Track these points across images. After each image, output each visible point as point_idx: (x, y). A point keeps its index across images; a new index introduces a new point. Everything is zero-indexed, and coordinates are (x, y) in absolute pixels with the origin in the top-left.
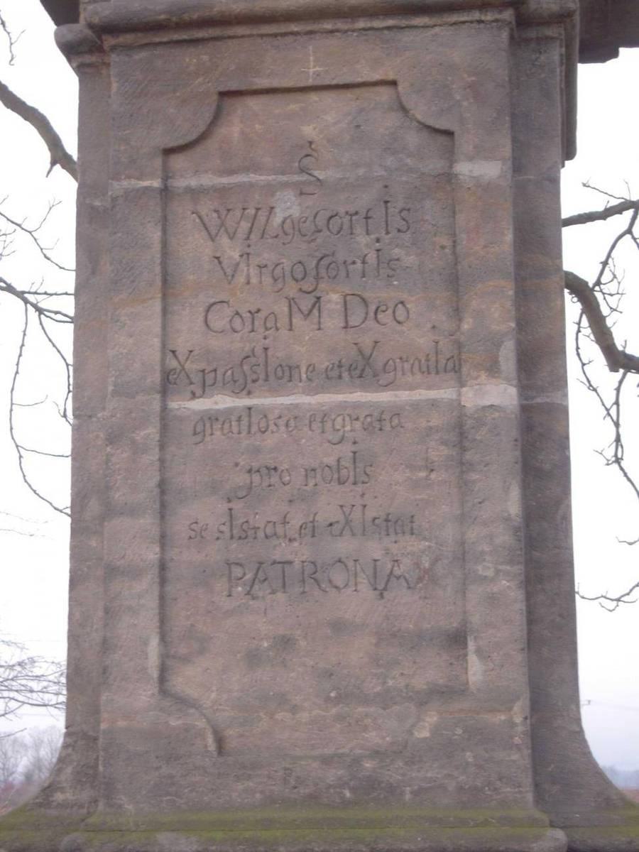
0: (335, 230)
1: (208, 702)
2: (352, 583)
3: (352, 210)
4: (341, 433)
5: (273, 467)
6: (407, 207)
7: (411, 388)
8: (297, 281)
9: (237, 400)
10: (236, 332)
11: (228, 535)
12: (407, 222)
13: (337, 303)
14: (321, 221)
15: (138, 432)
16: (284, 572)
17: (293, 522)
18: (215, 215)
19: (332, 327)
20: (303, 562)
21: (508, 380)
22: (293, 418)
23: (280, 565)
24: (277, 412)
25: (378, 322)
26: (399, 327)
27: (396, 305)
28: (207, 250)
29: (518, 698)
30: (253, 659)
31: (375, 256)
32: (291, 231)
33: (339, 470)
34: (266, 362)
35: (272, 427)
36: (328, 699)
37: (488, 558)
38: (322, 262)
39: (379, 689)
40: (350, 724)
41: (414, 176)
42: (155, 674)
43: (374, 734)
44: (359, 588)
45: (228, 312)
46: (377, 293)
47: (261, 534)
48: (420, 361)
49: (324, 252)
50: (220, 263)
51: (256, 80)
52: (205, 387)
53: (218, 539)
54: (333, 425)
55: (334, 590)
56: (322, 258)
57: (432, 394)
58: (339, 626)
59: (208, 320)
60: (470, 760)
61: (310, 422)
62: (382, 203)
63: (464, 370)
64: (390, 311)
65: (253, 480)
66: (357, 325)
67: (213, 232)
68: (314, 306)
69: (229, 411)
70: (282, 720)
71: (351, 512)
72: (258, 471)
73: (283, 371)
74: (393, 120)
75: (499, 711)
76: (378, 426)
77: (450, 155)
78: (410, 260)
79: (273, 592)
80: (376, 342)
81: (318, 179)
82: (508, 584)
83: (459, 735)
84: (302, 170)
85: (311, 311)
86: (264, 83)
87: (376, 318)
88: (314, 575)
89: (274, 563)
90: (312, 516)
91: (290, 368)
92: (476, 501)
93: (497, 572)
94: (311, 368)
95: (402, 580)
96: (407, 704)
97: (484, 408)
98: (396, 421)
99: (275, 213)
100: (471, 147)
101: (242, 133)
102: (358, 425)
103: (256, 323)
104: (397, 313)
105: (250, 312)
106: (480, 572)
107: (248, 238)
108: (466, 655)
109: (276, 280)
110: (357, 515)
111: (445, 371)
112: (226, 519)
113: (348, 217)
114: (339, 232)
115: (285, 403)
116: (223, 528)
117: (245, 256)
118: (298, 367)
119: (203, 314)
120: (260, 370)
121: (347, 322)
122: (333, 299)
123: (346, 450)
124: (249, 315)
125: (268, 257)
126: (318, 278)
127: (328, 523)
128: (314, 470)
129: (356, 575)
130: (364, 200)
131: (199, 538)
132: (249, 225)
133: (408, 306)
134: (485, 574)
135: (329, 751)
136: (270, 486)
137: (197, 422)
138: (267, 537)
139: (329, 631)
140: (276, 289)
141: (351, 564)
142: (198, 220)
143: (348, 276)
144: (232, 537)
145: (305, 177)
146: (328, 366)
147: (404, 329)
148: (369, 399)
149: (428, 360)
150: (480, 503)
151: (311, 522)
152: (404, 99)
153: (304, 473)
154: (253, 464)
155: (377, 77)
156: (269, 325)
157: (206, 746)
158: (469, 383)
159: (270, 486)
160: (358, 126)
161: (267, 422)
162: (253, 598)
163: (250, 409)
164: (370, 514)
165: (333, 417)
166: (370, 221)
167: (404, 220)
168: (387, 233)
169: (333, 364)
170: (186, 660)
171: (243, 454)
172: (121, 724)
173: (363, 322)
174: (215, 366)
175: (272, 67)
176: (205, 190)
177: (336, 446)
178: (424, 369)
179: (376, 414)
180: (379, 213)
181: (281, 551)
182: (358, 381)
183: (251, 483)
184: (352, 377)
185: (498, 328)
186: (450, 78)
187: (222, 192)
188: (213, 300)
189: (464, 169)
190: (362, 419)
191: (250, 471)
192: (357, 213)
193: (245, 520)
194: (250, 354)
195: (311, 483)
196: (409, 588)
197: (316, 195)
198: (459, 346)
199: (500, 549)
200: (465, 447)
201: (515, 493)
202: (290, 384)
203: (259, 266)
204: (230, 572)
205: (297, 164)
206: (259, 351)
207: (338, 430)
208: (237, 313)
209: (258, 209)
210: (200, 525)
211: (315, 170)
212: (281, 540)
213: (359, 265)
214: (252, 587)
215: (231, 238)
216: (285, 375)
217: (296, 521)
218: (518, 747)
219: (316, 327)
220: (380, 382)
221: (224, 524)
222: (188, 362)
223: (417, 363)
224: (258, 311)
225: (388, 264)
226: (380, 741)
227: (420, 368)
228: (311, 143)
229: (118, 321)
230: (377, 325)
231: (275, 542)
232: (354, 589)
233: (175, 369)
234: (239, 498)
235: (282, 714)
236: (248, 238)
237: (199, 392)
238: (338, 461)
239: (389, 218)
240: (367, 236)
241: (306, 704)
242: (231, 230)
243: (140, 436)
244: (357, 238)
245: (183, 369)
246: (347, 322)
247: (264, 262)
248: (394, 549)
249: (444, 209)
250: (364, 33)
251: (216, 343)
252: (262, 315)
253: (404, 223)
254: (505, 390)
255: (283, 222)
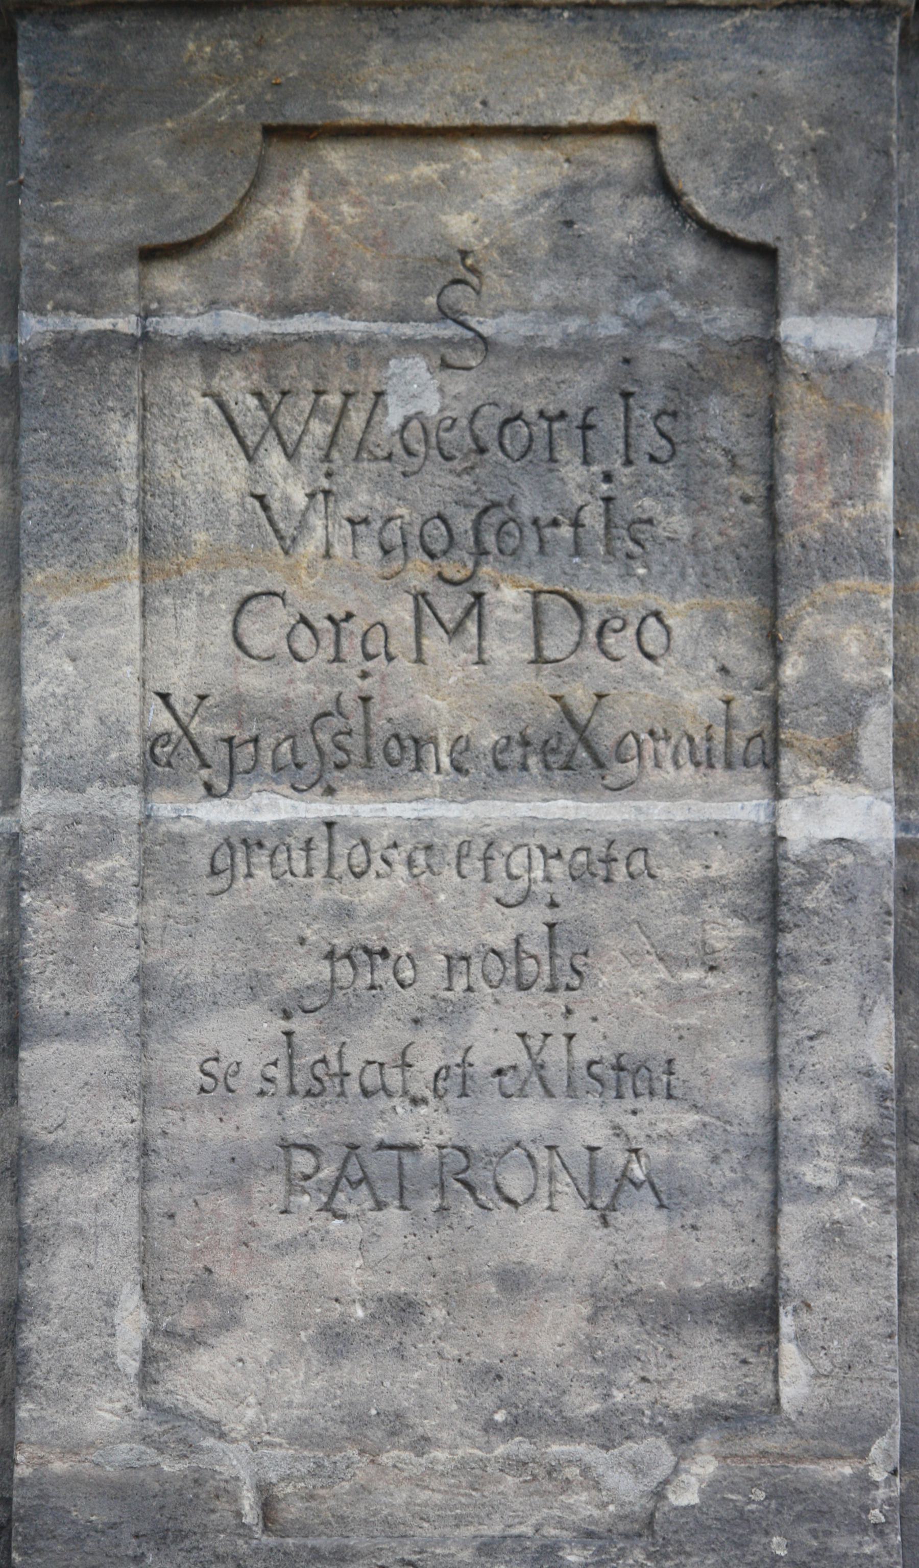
0: (515, 449)
1: (240, 1427)
2: (543, 1192)
3: (552, 410)
4: (522, 884)
5: (378, 948)
6: (671, 408)
7: (672, 794)
8: (432, 556)
9: (303, 805)
10: (301, 660)
11: (283, 1085)
12: (669, 440)
13: (516, 609)
14: (487, 431)
15: (89, 864)
16: (401, 1165)
17: (419, 1065)
18: (253, 402)
19: (507, 658)
20: (441, 1147)
21: (874, 787)
22: (425, 848)
23: (395, 1152)
24: (386, 837)
25: (605, 653)
26: (647, 665)
27: (644, 619)
28: (233, 475)
29: (881, 1432)
30: (336, 1341)
31: (601, 511)
32: (420, 448)
33: (518, 961)
34: (367, 726)
35: (378, 865)
36: (490, 1427)
37: (823, 1149)
38: (485, 519)
39: (594, 1407)
40: (535, 1477)
41: (688, 340)
42: (132, 1366)
43: (584, 1497)
44: (556, 1204)
45: (282, 616)
46: (607, 591)
47: (353, 1087)
48: (691, 740)
49: (489, 496)
50: (266, 508)
51: (344, 104)
52: (230, 772)
53: (262, 1093)
54: (507, 866)
55: (505, 1206)
56: (485, 510)
57: (715, 811)
58: (514, 1280)
59: (240, 631)
60: (782, 1552)
61: (459, 857)
62: (617, 397)
63: (786, 763)
64: (631, 632)
65: (338, 976)
66: (559, 657)
67: (251, 440)
68: (467, 613)
69: (284, 828)
70: (395, 1466)
71: (541, 1049)
72: (348, 956)
73: (403, 748)
74: (644, 210)
75: (841, 1457)
76: (602, 873)
77: (769, 295)
78: (678, 524)
79: (380, 1206)
80: (600, 696)
81: (479, 335)
82: (863, 1205)
83: (760, 1503)
84: (446, 314)
85: (460, 624)
86: (362, 112)
87: (600, 643)
88: (464, 1175)
89: (382, 1146)
90: (461, 1053)
91: (416, 741)
92: (803, 1033)
93: (844, 1178)
94: (462, 749)
95: (646, 1190)
96: (651, 1439)
97: (826, 842)
98: (638, 863)
99: (386, 407)
100: (811, 286)
101: (312, 220)
102: (558, 869)
103: (345, 643)
104: (646, 636)
105: (330, 618)
106: (809, 1178)
107: (327, 458)
108: (777, 1344)
109: (386, 552)
110: (555, 1054)
111: (746, 763)
112: (281, 1052)
113: (545, 424)
114: (523, 456)
115: (406, 815)
116: (272, 1071)
117: (320, 497)
118: (434, 741)
119: (230, 618)
120: (355, 744)
121: (538, 649)
122: (508, 599)
123: (534, 919)
124: (327, 624)
125: (362, 498)
126: (481, 552)
127: (493, 1068)
128: (466, 958)
129: (552, 1177)
130: (578, 387)
131: (221, 1089)
132: (330, 429)
133: (669, 622)
134: (817, 1183)
135: (494, 1529)
136: (373, 987)
137: (217, 849)
138: (366, 1093)
139: (493, 1290)
140: (387, 571)
141: (542, 1156)
142: (215, 410)
143: (542, 550)
144: (293, 1091)
145: (450, 330)
146: (497, 742)
147: (660, 671)
148: (582, 815)
149: (709, 739)
150: (811, 1038)
151: (458, 1065)
152: (670, 169)
153: (444, 964)
154: (335, 941)
155: (609, 115)
156: (371, 649)
157: (239, 1514)
158: (793, 792)
159: (373, 987)
160: (569, 224)
161: (368, 850)
162: (336, 1216)
163: (330, 825)
164: (583, 1052)
165: (507, 849)
166: (590, 434)
167: (663, 435)
168: (628, 462)
169: (508, 738)
170: (194, 1340)
171: (315, 918)
172: (59, 1466)
173: (572, 653)
174: (254, 732)
175: (380, 77)
176: (230, 344)
177: (514, 911)
178: (701, 755)
179: (599, 849)
180: (610, 422)
181: (408, 1124)
182: (558, 776)
183: (333, 980)
184: (548, 767)
185: (857, 678)
186: (770, 129)
187: (269, 352)
188: (249, 589)
189: (797, 331)
190: (567, 857)
191: (330, 956)
192: (562, 415)
193: (318, 1056)
194: (330, 707)
195: (460, 983)
196: (661, 1206)
197: (473, 372)
198: (775, 710)
199: (851, 1133)
200: (782, 922)
201: (883, 1018)
202: (416, 776)
203: (351, 521)
204: (289, 1163)
205: (432, 300)
206: (350, 703)
207: (517, 878)
208: (304, 620)
209: (347, 395)
210: (224, 1065)
211: (473, 315)
212: (396, 1101)
213: (566, 531)
214: (332, 1196)
215: (289, 456)
216: (403, 753)
217: (428, 1062)
218: (879, 1530)
219: (474, 657)
220: (609, 781)
221: (275, 1064)
222: (197, 719)
223: (685, 741)
224: (349, 616)
225: (628, 530)
226: (596, 1513)
227: (692, 754)
228: (464, 254)
229: (45, 623)
230: (603, 660)
231: (382, 1103)
232: (546, 1204)
233: (168, 734)
234: (306, 1012)
235: (395, 1453)
236: (327, 458)
237: (221, 785)
238: (517, 942)
239: (633, 431)
240: (581, 468)
241: (444, 1435)
242: (291, 439)
243: (94, 872)
244: (563, 470)
245: (186, 732)
246: (538, 649)
247: (363, 513)
248: (631, 1125)
249: (748, 416)
250: (587, 12)
251: (254, 680)
252: (356, 627)
253: (664, 442)
254: (869, 807)
255: (404, 427)
